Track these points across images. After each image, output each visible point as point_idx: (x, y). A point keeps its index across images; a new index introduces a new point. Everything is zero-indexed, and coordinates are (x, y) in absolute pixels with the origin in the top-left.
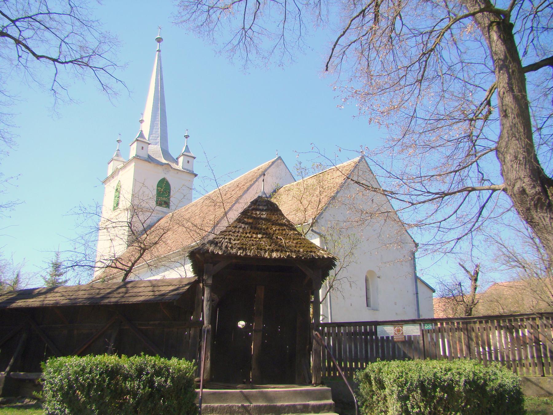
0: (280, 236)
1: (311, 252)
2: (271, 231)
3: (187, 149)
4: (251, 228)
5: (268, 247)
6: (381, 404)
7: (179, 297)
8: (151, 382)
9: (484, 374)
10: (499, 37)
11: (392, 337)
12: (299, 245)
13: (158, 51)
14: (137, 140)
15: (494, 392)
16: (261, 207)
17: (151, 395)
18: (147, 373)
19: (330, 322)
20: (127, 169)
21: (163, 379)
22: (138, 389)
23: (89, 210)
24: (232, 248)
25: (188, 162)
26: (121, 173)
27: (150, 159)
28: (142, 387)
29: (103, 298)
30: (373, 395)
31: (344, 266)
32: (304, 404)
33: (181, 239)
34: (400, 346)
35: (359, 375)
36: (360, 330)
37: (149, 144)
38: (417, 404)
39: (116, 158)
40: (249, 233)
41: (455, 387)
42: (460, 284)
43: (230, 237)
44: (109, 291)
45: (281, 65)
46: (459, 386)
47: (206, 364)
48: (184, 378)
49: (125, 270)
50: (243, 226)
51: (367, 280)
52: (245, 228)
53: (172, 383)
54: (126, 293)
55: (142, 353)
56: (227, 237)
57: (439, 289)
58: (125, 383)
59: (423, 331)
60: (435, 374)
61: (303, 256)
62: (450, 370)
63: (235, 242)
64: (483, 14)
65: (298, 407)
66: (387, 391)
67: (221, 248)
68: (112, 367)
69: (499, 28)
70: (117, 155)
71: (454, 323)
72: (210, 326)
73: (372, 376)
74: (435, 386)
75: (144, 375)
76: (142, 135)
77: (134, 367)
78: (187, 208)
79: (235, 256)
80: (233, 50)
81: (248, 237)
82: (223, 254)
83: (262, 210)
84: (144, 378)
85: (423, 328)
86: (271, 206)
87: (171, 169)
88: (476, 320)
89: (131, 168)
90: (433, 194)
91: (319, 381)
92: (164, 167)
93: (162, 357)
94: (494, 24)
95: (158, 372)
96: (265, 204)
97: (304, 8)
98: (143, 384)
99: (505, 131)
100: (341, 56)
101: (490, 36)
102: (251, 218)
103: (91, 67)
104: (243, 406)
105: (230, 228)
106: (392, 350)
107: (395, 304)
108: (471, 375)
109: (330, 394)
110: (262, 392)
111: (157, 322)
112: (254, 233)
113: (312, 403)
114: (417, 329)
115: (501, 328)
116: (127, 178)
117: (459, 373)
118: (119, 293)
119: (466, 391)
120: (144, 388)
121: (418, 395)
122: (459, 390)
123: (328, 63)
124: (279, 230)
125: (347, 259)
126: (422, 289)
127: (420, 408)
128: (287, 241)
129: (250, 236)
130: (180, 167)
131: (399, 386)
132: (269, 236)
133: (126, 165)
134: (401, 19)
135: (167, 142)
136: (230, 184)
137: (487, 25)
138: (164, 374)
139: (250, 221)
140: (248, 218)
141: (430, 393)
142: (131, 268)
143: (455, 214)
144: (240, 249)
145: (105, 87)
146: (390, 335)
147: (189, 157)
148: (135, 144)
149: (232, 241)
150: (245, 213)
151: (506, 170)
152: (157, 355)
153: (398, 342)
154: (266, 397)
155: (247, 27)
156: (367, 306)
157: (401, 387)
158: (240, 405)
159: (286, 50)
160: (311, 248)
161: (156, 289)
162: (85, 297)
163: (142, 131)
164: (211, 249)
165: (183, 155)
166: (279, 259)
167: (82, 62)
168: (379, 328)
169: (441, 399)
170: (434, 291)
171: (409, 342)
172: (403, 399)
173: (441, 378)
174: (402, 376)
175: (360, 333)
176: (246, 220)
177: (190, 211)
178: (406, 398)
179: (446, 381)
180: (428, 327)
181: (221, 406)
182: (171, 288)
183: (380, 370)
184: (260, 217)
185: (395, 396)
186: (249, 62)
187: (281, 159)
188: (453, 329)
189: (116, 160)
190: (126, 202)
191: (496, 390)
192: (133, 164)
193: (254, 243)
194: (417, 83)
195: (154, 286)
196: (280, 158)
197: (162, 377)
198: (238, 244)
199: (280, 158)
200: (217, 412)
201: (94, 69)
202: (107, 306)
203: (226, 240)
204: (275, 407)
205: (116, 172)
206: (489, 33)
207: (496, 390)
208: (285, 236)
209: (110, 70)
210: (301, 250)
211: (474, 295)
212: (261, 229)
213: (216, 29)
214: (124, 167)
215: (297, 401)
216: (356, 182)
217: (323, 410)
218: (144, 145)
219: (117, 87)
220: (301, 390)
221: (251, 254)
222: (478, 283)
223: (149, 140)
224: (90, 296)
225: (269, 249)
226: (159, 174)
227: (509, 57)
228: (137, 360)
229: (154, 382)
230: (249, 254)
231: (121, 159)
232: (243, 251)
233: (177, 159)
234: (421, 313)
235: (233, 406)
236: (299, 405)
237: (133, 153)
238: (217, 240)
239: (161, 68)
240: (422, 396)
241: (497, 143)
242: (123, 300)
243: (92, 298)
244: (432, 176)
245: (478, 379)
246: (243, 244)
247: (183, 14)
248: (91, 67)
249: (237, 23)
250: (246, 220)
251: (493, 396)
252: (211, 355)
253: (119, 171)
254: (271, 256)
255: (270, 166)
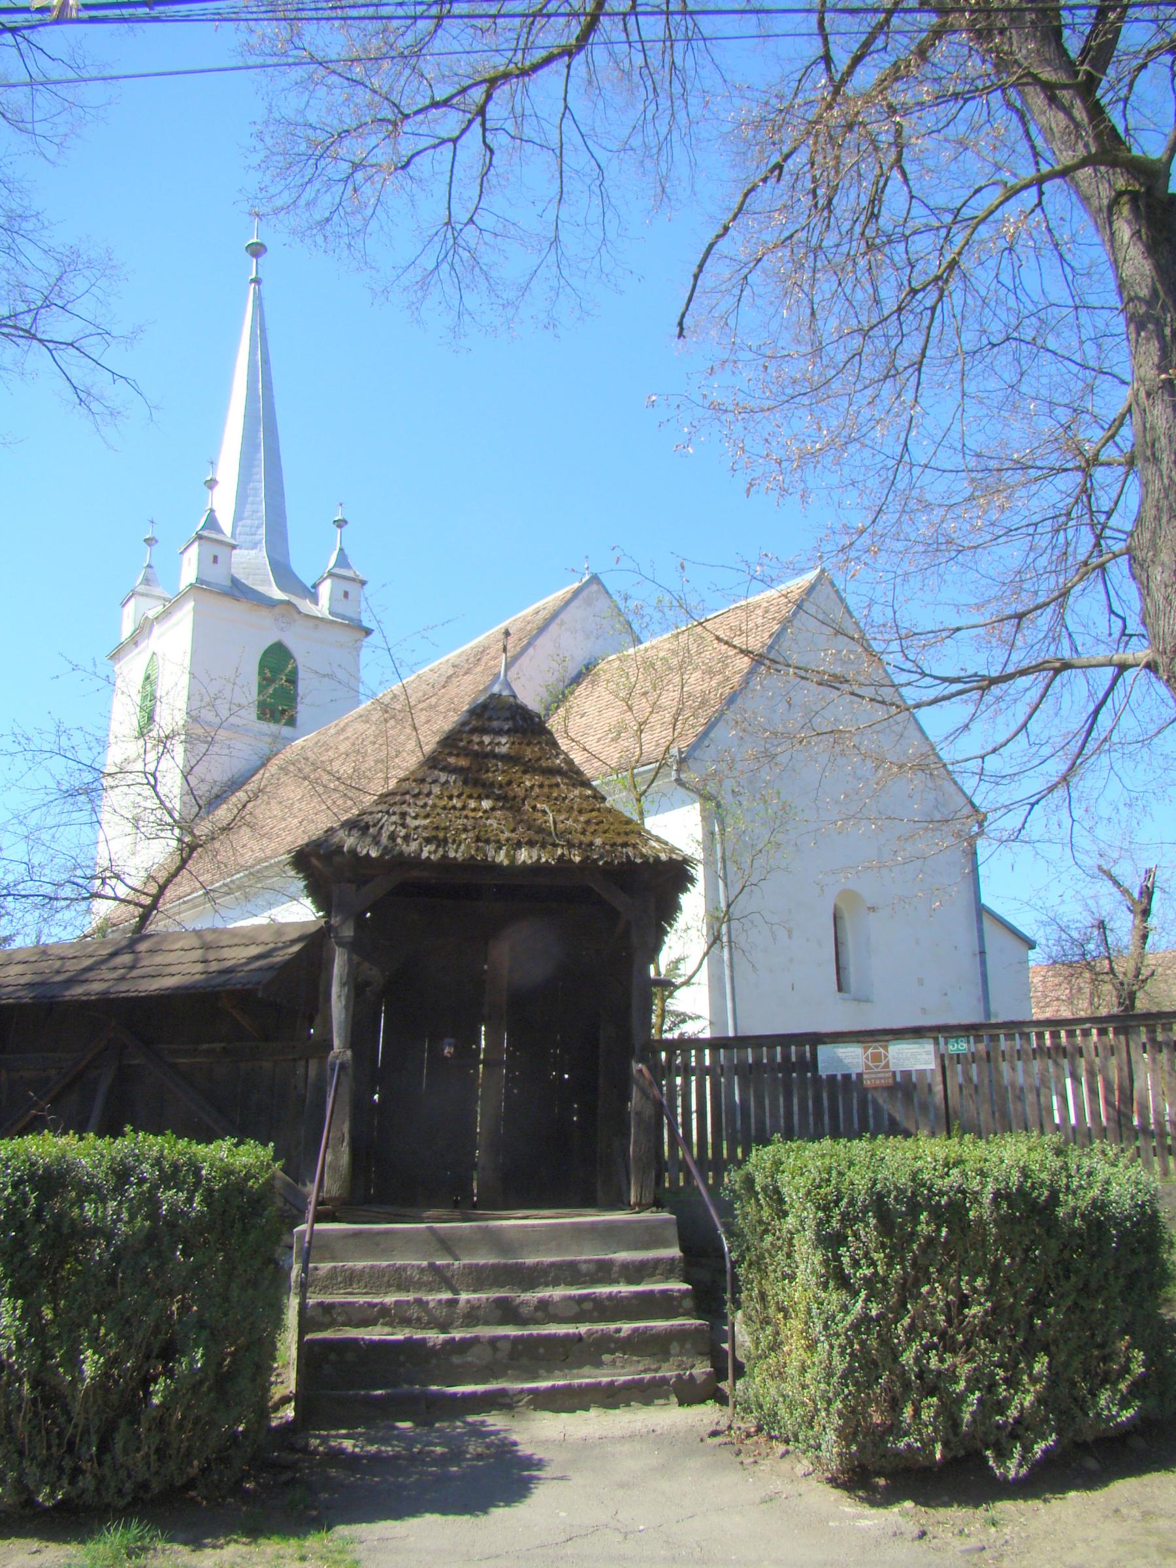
0: (543, 802)
1: (625, 845)
2: (520, 792)
3: (343, 561)
4: (465, 782)
5: (507, 834)
6: (780, 1256)
7: (269, 976)
8: (151, 1201)
9: (1053, 1174)
10: (1136, 234)
11: (860, 1075)
12: (591, 829)
13: (252, 281)
14: (199, 537)
15: (1077, 1222)
16: (495, 724)
17: (151, 1237)
18: (141, 1181)
19: (731, 1034)
20: (177, 616)
21: (182, 1196)
22: (115, 1222)
23: (37, 742)
24: (406, 838)
25: (346, 595)
26: (157, 630)
27: (237, 591)
28: (125, 1216)
29: (71, 982)
30: (766, 1231)
31: (754, 879)
32: (599, 1261)
33: (296, 816)
34: (880, 1101)
35: (732, 1178)
36: (772, 1058)
37: (234, 547)
38: (866, 1255)
39: (142, 589)
40: (459, 796)
41: (969, 1209)
42: (1101, 925)
43: (405, 808)
44: (88, 962)
45: (551, 324)
46: (980, 1204)
47: (334, 1158)
48: (241, 1192)
49: (141, 906)
50: (443, 777)
51: (837, 918)
52: (447, 782)
53: (208, 1205)
54: (133, 967)
55: (128, 1128)
56: (396, 809)
57: (1043, 941)
58: (82, 1208)
59: (942, 1057)
60: (914, 1176)
61: (601, 857)
62: (959, 1162)
63: (417, 823)
64: (1095, 171)
65: (584, 1267)
66: (791, 1221)
67: (376, 841)
68: (47, 1168)
69: (1135, 209)
70: (147, 581)
71: (1028, 1035)
72: (349, 1053)
73: (759, 1180)
74: (914, 1208)
75: (131, 1184)
76: (212, 523)
77: (106, 1164)
78: (342, 725)
79: (415, 862)
80: (424, 284)
81: (454, 807)
82: (382, 856)
83: (499, 732)
84: (132, 1192)
85: (942, 1050)
86: (524, 719)
87: (296, 616)
88: (1087, 1026)
89: (185, 616)
90: (944, 680)
91: (648, 1198)
92: (277, 610)
93: (180, 1137)
94: (1125, 198)
95: (171, 1176)
96: (508, 714)
97: (615, 162)
98: (129, 1210)
99: (1149, 503)
100: (736, 292)
101: (1112, 234)
102: (467, 755)
103: (41, 341)
104: (432, 1266)
105: (406, 785)
106: (847, 1110)
107: (921, 982)
108: (1015, 1178)
109: (673, 1233)
110: (488, 1231)
111: (218, 1046)
112: (470, 797)
113: (623, 1256)
114: (928, 1053)
115: (1158, 1047)
116: (174, 644)
117: (982, 1173)
118: (115, 968)
119: (1001, 1222)
120: (132, 1217)
121: (868, 1230)
122: (980, 1217)
123: (683, 316)
124: (541, 786)
125: (761, 861)
126: (994, 937)
127: (875, 1266)
128: (562, 818)
129: (459, 805)
130: (322, 608)
131: (818, 1208)
132: (508, 802)
133: (170, 608)
134: (906, 180)
135: (286, 540)
136: (459, 656)
137: (1105, 202)
138: (184, 1182)
139: (463, 762)
140: (457, 755)
141: (902, 1227)
142: (157, 898)
143: (1022, 737)
144: (428, 841)
145: (82, 396)
146: (854, 1072)
147: (348, 580)
148: (195, 549)
149: (408, 820)
150: (450, 742)
151: (1152, 612)
152: (168, 1132)
153: (875, 1088)
154: (496, 1241)
155: (461, 216)
156: (840, 989)
157: (826, 1208)
158: (425, 1263)
159: (562, 281)
160: (627, 834)
161: (212, 955)
162: (23, 981)
163: (212, 511)
164: (349, 842)
165: (331, 575)
166: (537, 869)
167: (15, 327)
168: (823, 1051)
169: (931, 1241)
170: (1031, 945)
171: (905, 1087)
172: (830, 1241)
173: (932, 1185)
174: (829, 1180)
175: (772, 1066)
176: (452, 760)
177: (349, 732)
178: (838, 1240)
179: (946, 1193)
180: (959, 1046)
181: (372, 1267)
182: (254, 951)
183: (777, 1163)
184: (492, 751)
185: (809, 1234)
186: (466, 318)
187: (600, 583)
188: (1026, 1053)
189: (142, 595)
190: (172, 713)
191: (1083, 1216)
192: (189, 606)
193: (470, 823)
194: (910, 370)
195: (207, 947)
196: (595, 579)
197: (180, 1190)
198: (425, 828)
199: (595, 579)
200: (362, 1284)
201: (51, 346)
202: (82, 1006)
203: (394, 818)
204: (520, 1268)
205: (143, 629)
206: (1111, 224)
207: (1083, 1216)
208: (558, 803)
209: (93, 346)
210: (598, 841)
211: (1142, 956)
212: (492, 785)
213: (373, 225)
214: (166, 614)
215: (581, 1254)
216: (742, 651)
217: (652, 1275)
218: (220, 551)
219: (118, 394)
220: (593, 1223)
221: (459, 855)
222: (1153, 921)
223: (233, 536)
224: (38, 979)
225: (508, 840)
226: (264, 633)
227: (1162, 294)
228: (122, 1146)
229: (157, 1204)
230: (452, 854)
231: (157, 591)
232: (438, 846)
233: (315, 586)
234: (993, 1007)
235: (404, 1268)
236: (585, 1261)
237: (189, 573)
238: (367, 818)
239: (263, 331)
240: (880, 1234)
241: (1130, 535)
242: (123, 987)
243: (43, 984)
244: (958, 629)
245: (1033, 1187)
246: (437, 828)
247: (273, 190)
248: (41, 341)
249: (432, 210)
250: (452, 760)
251: (1074, 1232)
252: (351, 1131)
253: (152, 626)
254: (513, 859)
255: (567, 603)
